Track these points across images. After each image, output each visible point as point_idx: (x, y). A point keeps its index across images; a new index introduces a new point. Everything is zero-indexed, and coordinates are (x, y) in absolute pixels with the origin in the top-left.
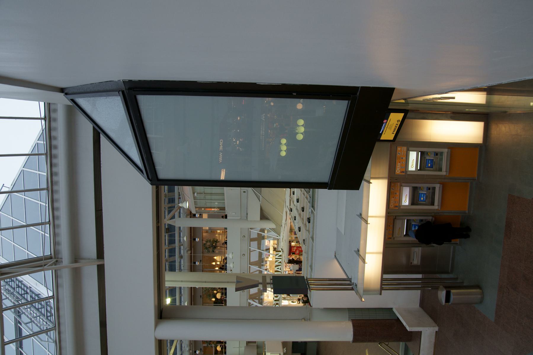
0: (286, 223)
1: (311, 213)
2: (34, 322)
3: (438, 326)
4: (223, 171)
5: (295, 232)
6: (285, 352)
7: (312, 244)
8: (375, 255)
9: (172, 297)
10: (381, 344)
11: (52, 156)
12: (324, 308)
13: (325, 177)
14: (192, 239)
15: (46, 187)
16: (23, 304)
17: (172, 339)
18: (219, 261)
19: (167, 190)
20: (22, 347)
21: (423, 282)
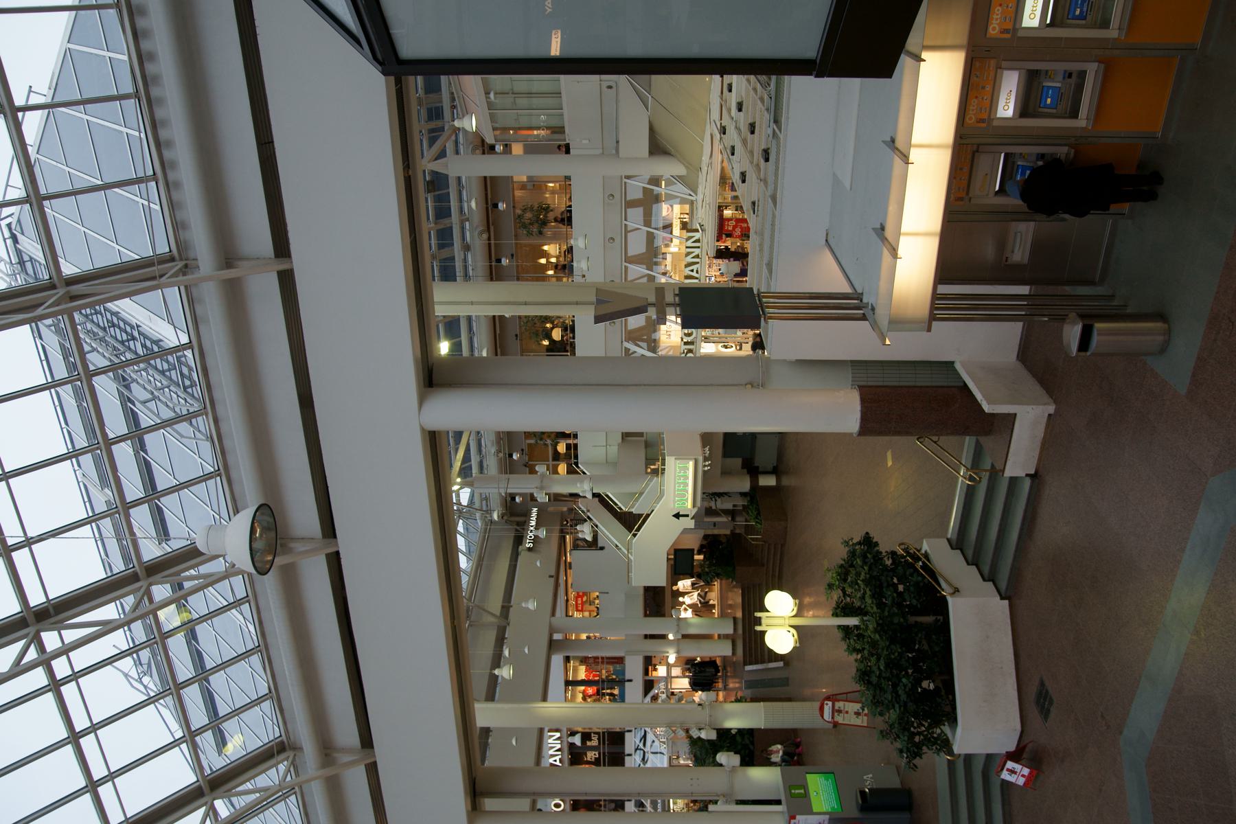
0: (711, 161)
1: (771, 136)
2: (160, 400)
4: (555, 34)
5: (733, 184)
6: (707, 455)
7: (771, 213)
8: (920, 239)
9: (453, 339)
11: (134, 11)
12: (798, 361)
13: (809, 45)
14: (490, 206)
15: (132, 91)
16: (129, 363)
17: (459, 429)
18: (554, 255)
19: (421, 89)
21: (1030, 303)
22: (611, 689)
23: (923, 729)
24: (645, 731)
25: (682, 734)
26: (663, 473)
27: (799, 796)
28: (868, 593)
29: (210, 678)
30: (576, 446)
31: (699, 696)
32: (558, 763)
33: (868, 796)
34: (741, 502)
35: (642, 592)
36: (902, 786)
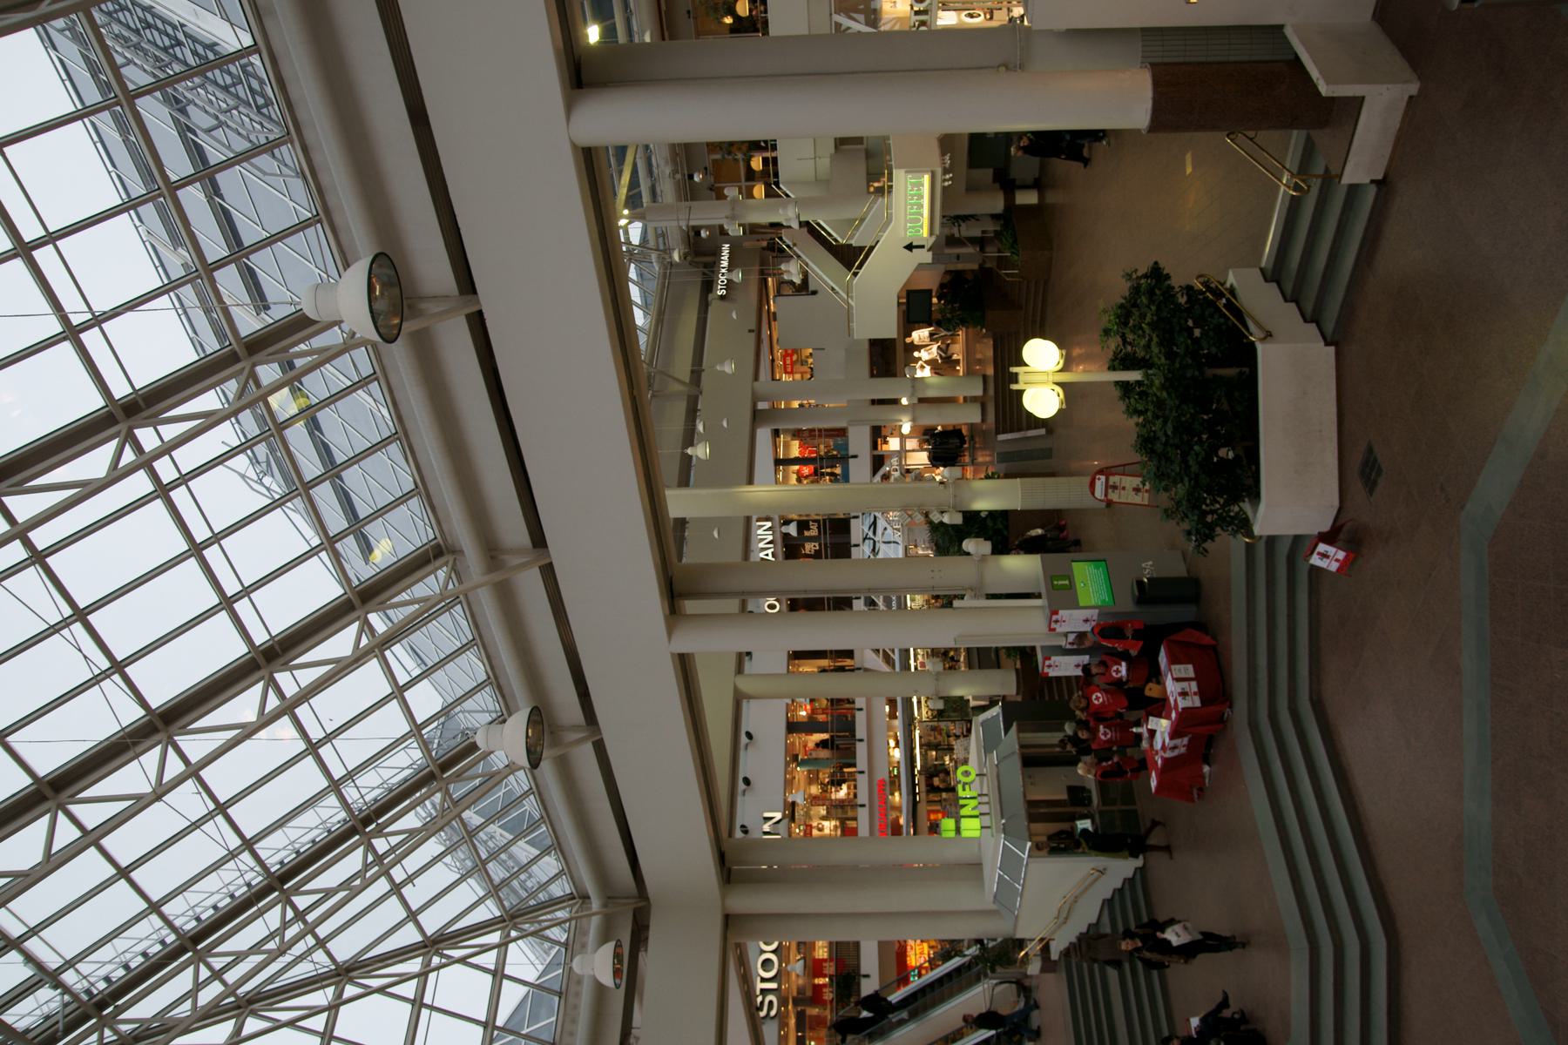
2: (228, 126)
3: (1420, 79)
6: (947, 166)
10: (1232, 136)
20: (222, 194)
22: (832, 467)
23: (1218, 506)
24: (875, 517)
25: (920, 518)
26: (890, 192)
27: (1063, 587)
28: (1155, 339)
29: (343, 474)
30: (775, 160)
31: (940, 473)
32: (770, 558)
33: (1147, 586)
34: (992, 227)
35: (866, 346)
36: (1188, 571)
